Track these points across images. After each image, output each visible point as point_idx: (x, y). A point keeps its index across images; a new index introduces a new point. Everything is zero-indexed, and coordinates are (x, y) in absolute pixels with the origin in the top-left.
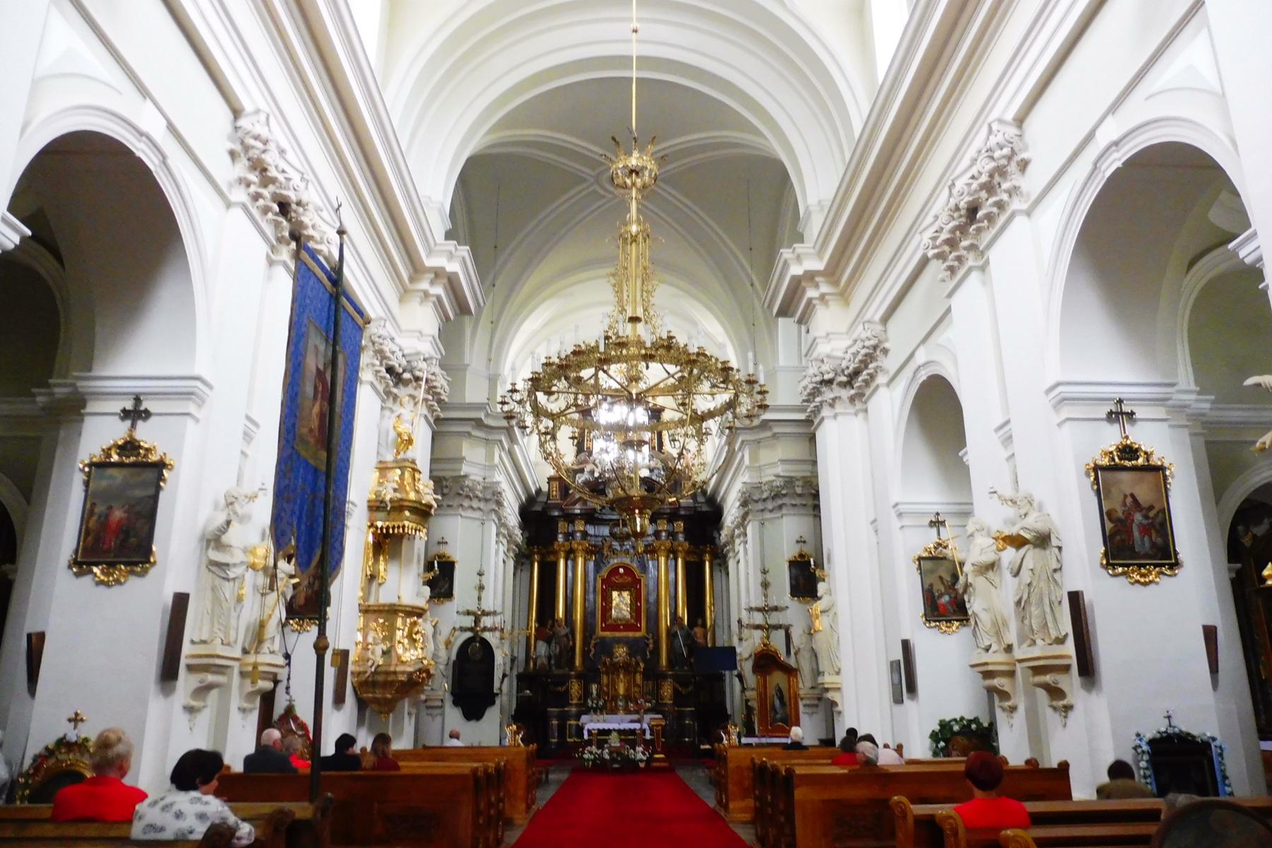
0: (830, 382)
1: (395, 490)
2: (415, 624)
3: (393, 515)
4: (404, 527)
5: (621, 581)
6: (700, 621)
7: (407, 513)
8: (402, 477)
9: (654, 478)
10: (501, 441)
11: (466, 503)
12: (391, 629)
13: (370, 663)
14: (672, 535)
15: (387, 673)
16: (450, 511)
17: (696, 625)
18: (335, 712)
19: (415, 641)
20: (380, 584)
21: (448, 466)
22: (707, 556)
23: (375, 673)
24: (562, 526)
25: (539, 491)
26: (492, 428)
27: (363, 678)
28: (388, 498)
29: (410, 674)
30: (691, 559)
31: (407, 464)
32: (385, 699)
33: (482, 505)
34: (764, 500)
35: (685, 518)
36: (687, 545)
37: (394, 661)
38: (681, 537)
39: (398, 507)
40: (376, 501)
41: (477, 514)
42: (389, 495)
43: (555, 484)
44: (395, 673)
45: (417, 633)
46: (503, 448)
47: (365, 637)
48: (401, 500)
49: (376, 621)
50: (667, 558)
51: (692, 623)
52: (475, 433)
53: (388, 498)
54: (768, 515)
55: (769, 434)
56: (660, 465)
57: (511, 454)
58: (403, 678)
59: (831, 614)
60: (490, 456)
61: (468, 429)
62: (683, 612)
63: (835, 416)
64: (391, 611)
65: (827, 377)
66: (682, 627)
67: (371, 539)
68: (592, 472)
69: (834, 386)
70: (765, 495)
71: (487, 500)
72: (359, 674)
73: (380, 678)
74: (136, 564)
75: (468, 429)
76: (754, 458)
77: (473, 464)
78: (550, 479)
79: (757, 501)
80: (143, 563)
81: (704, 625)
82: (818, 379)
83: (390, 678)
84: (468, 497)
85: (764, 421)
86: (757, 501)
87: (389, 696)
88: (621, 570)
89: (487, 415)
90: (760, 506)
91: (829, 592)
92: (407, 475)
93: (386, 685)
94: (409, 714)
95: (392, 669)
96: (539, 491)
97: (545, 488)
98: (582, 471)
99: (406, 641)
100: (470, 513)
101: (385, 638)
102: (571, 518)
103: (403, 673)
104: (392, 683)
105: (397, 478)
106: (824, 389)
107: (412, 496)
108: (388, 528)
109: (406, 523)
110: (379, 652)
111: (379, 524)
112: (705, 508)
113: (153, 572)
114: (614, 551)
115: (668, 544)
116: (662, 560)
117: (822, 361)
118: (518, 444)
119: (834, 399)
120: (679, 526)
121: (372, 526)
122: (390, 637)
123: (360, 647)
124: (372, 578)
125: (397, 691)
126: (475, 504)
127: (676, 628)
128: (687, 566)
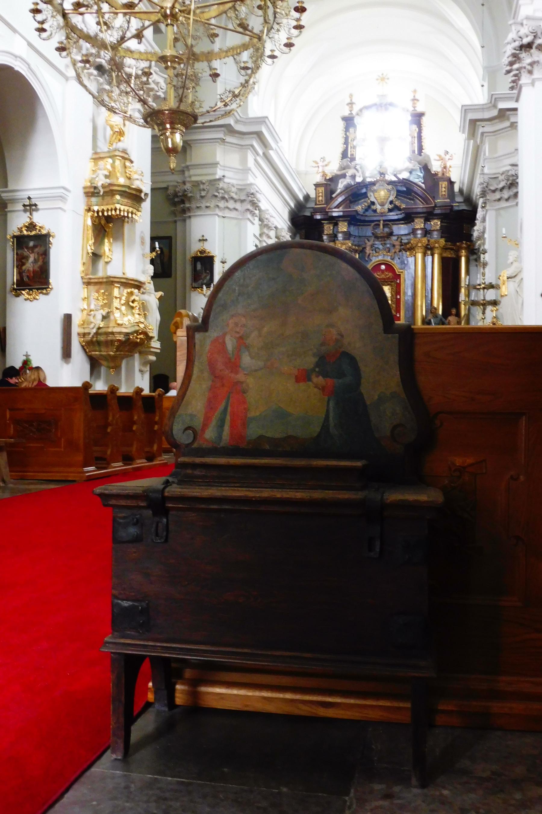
0: (529, 46)
1: (106, 177)
2: (132, 294)
3: (108, 199)
4: (116, 210)
5: (383, 276)
6: (454, 311)
7: (118, 197)
8: (113, 165)
9: (411, 179)
10: (252, 146)
11: (222, 204)
12: (110, 297)
13: (92, 326)
14: (426, 232)
15: (107, 334)
16: (208, 212)
17: (451, 314)
18: (65, 365)
19: (132, 308)
20: (107, 263)
21: (204, 171)
22: (463, 253)
23: (97, 334)
24: (328, 229)
25: (307, 198)
26: (243, 134)
27: (88, 338)
28: (99, 184)
29: (127, 334)
30: (447, 254)
31: (117, 153)
32: (109, 355)
33: (238, 206)
34: (502, 189)
35: (443, 217)
36: (442, 241)
37: (112, 324)
38: (435, 235)
39: (110, 192)
40: (91, 187)
41: (233, 214)
42: (101, 181)
43: (321, 190)
44: (113, 333)
45: (133, 301)
46: (258, 154)
47: (89, 305)
48: (110, 185)
49: (97, 292)
50: (425, 255)
51: (446, 313)
52: (229, 139)
53: (99, 184)
54: (503, 204)
55: (507, 124)
56: (417, 167)
57: (267, 157)
58: (121, 338)
59: (517, 279)
60: (244, 160)
61: (221, 135)
62: (438, 303)
63: (533, 84)
64: (110, 282)
65: (526, 41)
66: (435, 316)
67: (89, 222)
68: (353, 177)
69: (534, 51)
70: (501, 186)
71: (242, 201)
72: (84, 335)
73: (102, 338)
74: (43, 289)
75: (221, 135)
76: (493, 149)
77: (225, 168)
78: (317, 185)
79: (494, 191)
80: (46, 288)
81: (458, 314)
82: (517, 44)
83: (110, 338)
84: (223, 198)
85: (501, 110)
86: (494, 191)
87: (112, 353)
88: (383, 267)
89: (237, 121)
90: (497, 195)
91: (518, 259)
92: (118, 163)
93: (109, 344)
94: (141, 371)
95: (110, 330)
96: (307, 198)
97: (313, 195)
98: (344, 176)
99: (123, 308)
100: (227, 213)
101: (103, 307)
102: (334, 221)
103: (120, 333)
104: (112, 342)
105: (109, 167)
106: (523, 55)
107: (122, 181)
108: (103, 211)
109: (118, 206)
110: (99, 317)
111: (96, 208)
112: (464, 207)
113: (52, 293)
114: (376, 250)
115: (425, 240)
116: (419, 256)
117: (522, 24)
118: (272, 149)
119: (532, 64)
120: (436, 224)
121: (89, 210)
122: (109, 305)
123: (85, 312)
124: (96, 256)
125: (118, 349)
126: (231, 204)
127: (430, 317)
128: (444, 261)
